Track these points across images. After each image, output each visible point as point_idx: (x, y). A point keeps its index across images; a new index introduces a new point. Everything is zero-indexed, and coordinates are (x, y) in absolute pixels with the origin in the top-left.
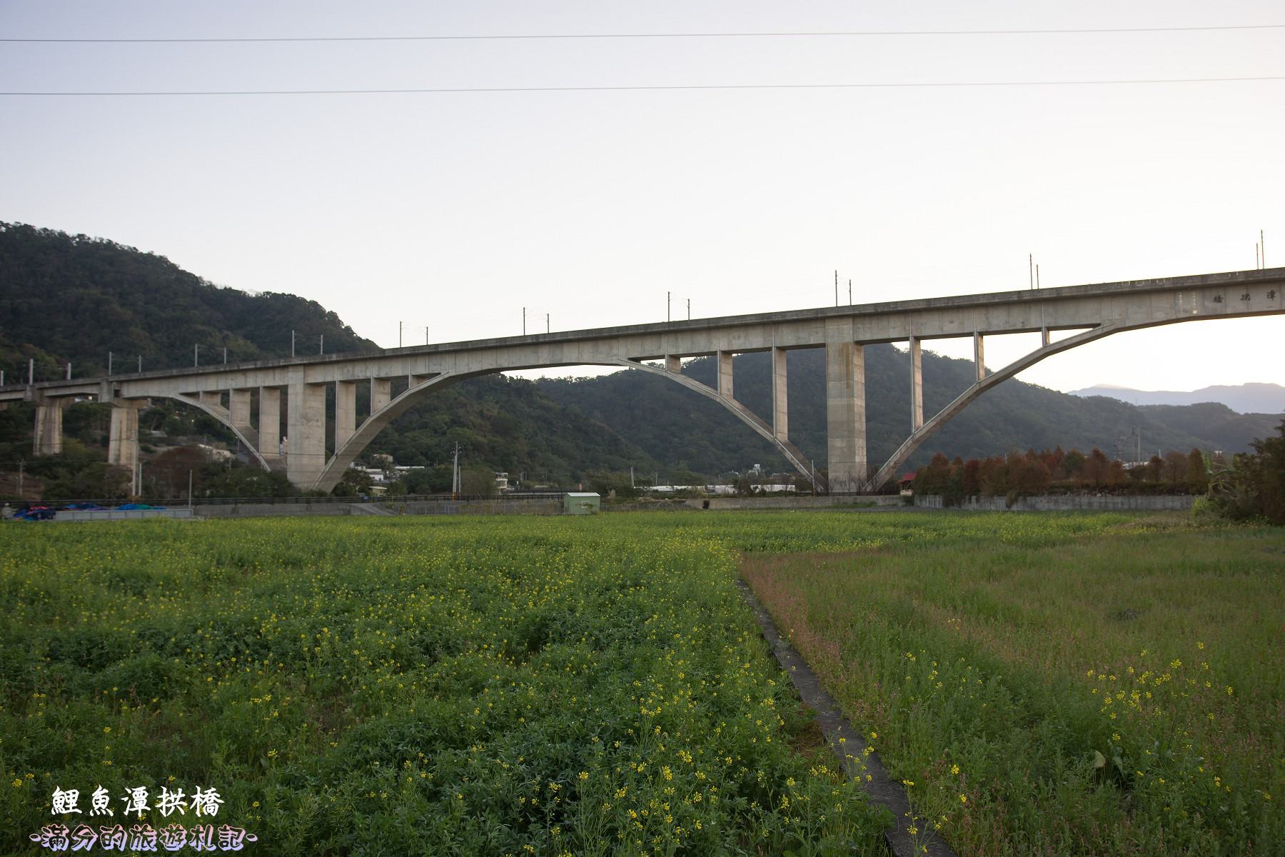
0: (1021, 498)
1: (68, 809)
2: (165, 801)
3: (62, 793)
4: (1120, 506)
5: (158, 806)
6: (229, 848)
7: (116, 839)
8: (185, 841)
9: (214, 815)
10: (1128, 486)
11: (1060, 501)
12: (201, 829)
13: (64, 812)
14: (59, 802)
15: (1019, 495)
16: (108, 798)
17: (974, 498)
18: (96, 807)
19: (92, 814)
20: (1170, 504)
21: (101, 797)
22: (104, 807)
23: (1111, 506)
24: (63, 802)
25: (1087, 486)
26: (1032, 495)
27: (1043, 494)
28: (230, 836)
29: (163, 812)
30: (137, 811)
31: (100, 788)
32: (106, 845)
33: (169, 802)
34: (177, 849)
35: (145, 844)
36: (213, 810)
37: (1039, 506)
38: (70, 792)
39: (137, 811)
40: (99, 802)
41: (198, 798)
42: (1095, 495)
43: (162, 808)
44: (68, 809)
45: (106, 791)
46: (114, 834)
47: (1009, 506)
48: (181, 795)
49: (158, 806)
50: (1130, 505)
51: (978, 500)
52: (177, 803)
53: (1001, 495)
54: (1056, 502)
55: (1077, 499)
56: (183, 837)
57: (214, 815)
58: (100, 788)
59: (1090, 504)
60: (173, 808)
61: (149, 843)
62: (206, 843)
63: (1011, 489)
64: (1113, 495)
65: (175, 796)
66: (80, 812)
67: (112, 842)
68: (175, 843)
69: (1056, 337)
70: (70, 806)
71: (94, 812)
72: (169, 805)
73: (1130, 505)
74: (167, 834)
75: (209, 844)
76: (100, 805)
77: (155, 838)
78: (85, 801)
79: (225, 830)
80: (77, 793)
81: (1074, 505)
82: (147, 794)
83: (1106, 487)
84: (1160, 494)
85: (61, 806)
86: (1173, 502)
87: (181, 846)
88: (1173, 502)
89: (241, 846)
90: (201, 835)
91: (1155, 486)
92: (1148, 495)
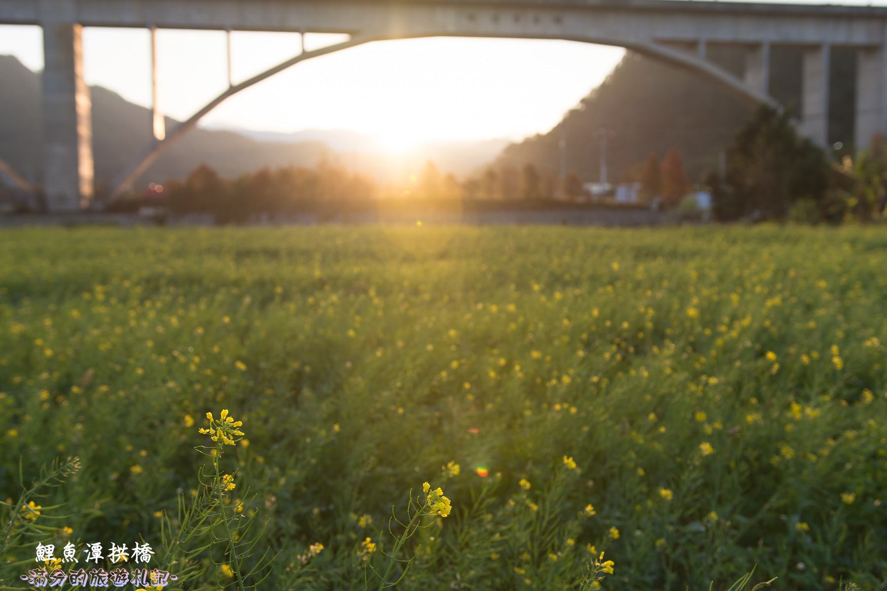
3: (43, 547)
9: (148, 562)
16: (74, 551)
18: (66, 556)
22: (72, 556)
29: (113, 560)
31: (69, 543)
33: (117, 553)
34: (122, 585)
35: (100, 582)
36: (146, 558)
38: (48, 546)
41: (136, 550)
48: (125, 548)
56: (127, 577)
57: (148, 562)
58: (69, 543)
61: (103, 581)
65: (121, 549)
69: (315, 41)
72: (116, 555)
76: (69, 555)
85: (42, 556)
87: (125, 583)
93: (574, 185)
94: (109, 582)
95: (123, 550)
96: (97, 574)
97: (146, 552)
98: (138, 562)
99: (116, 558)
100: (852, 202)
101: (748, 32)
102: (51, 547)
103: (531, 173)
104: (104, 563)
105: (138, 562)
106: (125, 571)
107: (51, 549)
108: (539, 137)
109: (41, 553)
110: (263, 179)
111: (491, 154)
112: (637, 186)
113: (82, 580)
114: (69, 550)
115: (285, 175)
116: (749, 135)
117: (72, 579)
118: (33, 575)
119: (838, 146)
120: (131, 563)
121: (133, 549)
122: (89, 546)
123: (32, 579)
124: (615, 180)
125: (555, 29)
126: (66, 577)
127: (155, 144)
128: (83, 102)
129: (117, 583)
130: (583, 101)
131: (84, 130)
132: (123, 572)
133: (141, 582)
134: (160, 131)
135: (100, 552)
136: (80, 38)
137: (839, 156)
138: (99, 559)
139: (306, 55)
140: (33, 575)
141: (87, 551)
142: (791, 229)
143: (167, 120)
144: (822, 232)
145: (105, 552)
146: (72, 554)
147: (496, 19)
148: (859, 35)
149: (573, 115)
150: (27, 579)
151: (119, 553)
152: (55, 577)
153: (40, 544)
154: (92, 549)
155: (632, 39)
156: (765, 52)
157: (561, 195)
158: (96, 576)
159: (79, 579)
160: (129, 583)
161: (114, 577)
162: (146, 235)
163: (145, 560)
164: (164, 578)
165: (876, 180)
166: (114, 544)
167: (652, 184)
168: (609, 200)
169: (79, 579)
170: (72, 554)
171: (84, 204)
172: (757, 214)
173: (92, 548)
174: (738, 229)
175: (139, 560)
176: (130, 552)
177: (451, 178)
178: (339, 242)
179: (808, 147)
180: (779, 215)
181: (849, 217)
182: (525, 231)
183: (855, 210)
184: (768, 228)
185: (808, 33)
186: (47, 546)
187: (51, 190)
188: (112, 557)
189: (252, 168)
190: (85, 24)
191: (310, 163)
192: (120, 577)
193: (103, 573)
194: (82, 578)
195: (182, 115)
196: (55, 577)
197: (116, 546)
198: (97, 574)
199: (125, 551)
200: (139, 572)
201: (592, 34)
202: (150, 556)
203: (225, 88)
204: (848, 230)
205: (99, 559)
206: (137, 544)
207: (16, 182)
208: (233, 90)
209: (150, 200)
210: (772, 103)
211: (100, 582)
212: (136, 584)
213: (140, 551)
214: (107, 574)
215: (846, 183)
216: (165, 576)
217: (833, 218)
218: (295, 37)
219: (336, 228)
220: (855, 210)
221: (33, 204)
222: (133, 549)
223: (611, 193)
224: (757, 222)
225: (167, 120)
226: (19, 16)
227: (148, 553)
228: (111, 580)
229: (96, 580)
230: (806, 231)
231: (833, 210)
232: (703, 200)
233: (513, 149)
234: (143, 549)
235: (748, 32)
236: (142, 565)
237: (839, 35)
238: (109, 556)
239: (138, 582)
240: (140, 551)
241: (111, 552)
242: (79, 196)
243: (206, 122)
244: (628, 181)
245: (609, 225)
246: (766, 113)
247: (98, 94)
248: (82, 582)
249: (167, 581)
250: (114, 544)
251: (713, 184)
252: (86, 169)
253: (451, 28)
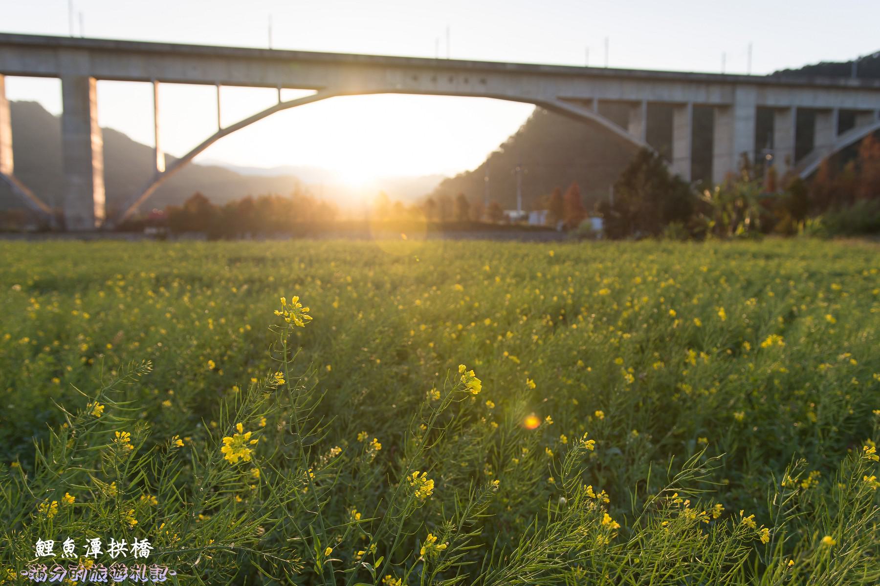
1: (47, 553)
3: (42, 542)
9: (146, 557)
13: (44, 555)
16: (74, 546)
18: (66, 552)
22: (71, 551)
28: (157, 572)
29: (112, 555)
31: (69, 539)
33: (116, 548)
34: (121, 580)
35: (100, 577)
36: (145, 554)
38: (48, 541)
41: (135, 545)
44: (47, 553)
45: (72, 541)
48: (124, 544)
52: (121, 549)
56: (125, 572)
57: (146, 557)
58: (69, 539)
60: (119, 553)
61: (102, 576)
62: (141, 577)
65: (120, 544)
68: (120, 577)
69: (289, 95)
70: (48, 551)
72: (115, 551)
76: (68, 551)
77: (106, 573)
85: (42, 551)
87: (124, 578)
93: (496, 211)
94: (108, 578)
95: (122, 545)
96: (97, 569)
97: (145, 548)
98: (136, 557)
99: (115, 553)
100: (712, 224)
101: (631, 93)
102: (51, 542)
103: (463, 201)
104: (102, 560)
105: (136, 557)
106: (124, 566)
107: (50, 544)
108: (468, 173)
109: (40, 548)
110: (247, 204)
111: (430, 187)
112: (546, 212)
113: (82, 575)
114: (69, 545)
115: (266, 202)
116: (633, 171)
117: (71, 574)
118: (33, 571)
119: (700, 182)
120: (128, 560)
121: (132, 545)
122: (89, 541)
123: (32, 574)
124: (528, 208)
125: (481, 89)
126: (66, 572)
127: (158, 176)
128: (97, 141)
129: (116, 578)
130: (503, 146)
131: (98, 164)
132: (122, 567)
133: (139, 577)
134: (161, 166)
135: (100, 548)
136: (95, 88)
137: (702, 191)
138: (98, 555)
139: (282, 106)
140: (33, 571)
141: (86, 546)
142: (666, 244)
143: (167, 156)
144: (690, 245)
145: (104, 547)
146: (71, 549)
147: (434, 80)
148: (715, 96)
149: (495, 155)
150: (26, 574)
151: (117, 547)
152: (55, 572)
153: (40, 539)
154: (92, 545)
155: (541, 98)
156: (644, 108)
157: (486, 219)
158: (95, 571)
159: (79, 574)
160: (128, 579)
161: (113, 572)
162: (152, 248)
163: (144, 555)
164: (162, 573)
165: (730, 207)
166: (113, 540)
167: (557, 211)
168: (523, 223)
169: (79, 574)
170: (71, 549)
171: (98, 224)
172: (638, 234)
173: (91, 543)
174: (625, 244)
175: (138, 555)
176: (129, 546)
177: (398, 205)
178: (312, 252)
179: (677, 181)
180: (656, 233)
181: (709, 235)
182: (460, 244)
183: (713, 230)
184: (648, 243)
185: (677, 94)
186: (47, 542)
187: (69, 213)
188: (111, 552)
189: (237, 196)
190: (98, 78)
191: (286, 193)
192: (119, 572)
193: (102, 568)
194: (81, 573)
195: (179, 153)
196: (55, 572)
197: (115, 542)
198: (97, 569)
199: (124, 546)
200: (138, 567)
201: (510, 93)
202: (149, 551)
203: (214, 130)
204: (710, 244)
205: (98, 555)
206: (136, 539)
207: (41, 206)
208: (222, 133)
209: (152, 221)
210: (651, 149)
211: (100, 577)
212: (135, 579)
213: (139, 546)
214: (106, 569)
215: (707, 209)
216: (164, 570)
217: (699, 236)
218: (273, 91)
219: (310, 242)
220: (713, 230)
221: (53, 224)
222: (132, 545)
223: (526, 218)
224: (639, 239)
225: (167, 156)
226: (42, 69)
227: (147, 548)
228: (111, 575)
229: (95, 575)
230: (677, 245)
231: (696, 230)
232: (597, 223)
233: (447, 182)
234: (141, 545)
235: (631, 93)
236: (141, 560)
237: (700, 96)
238: (109, 551)
239: (137, 577)
240: (139, 546)
241: (110, 547)
242: (93, 218)
243: (198, 159)
244: (539, 208)
245: (525, 240)
246: (645, 155)
247: (108, 134)
248: (81, 577)
249: (166, 576)
250: (113, 540)
251: (605, 211)
252: (99, 195)
253: (399, 87)
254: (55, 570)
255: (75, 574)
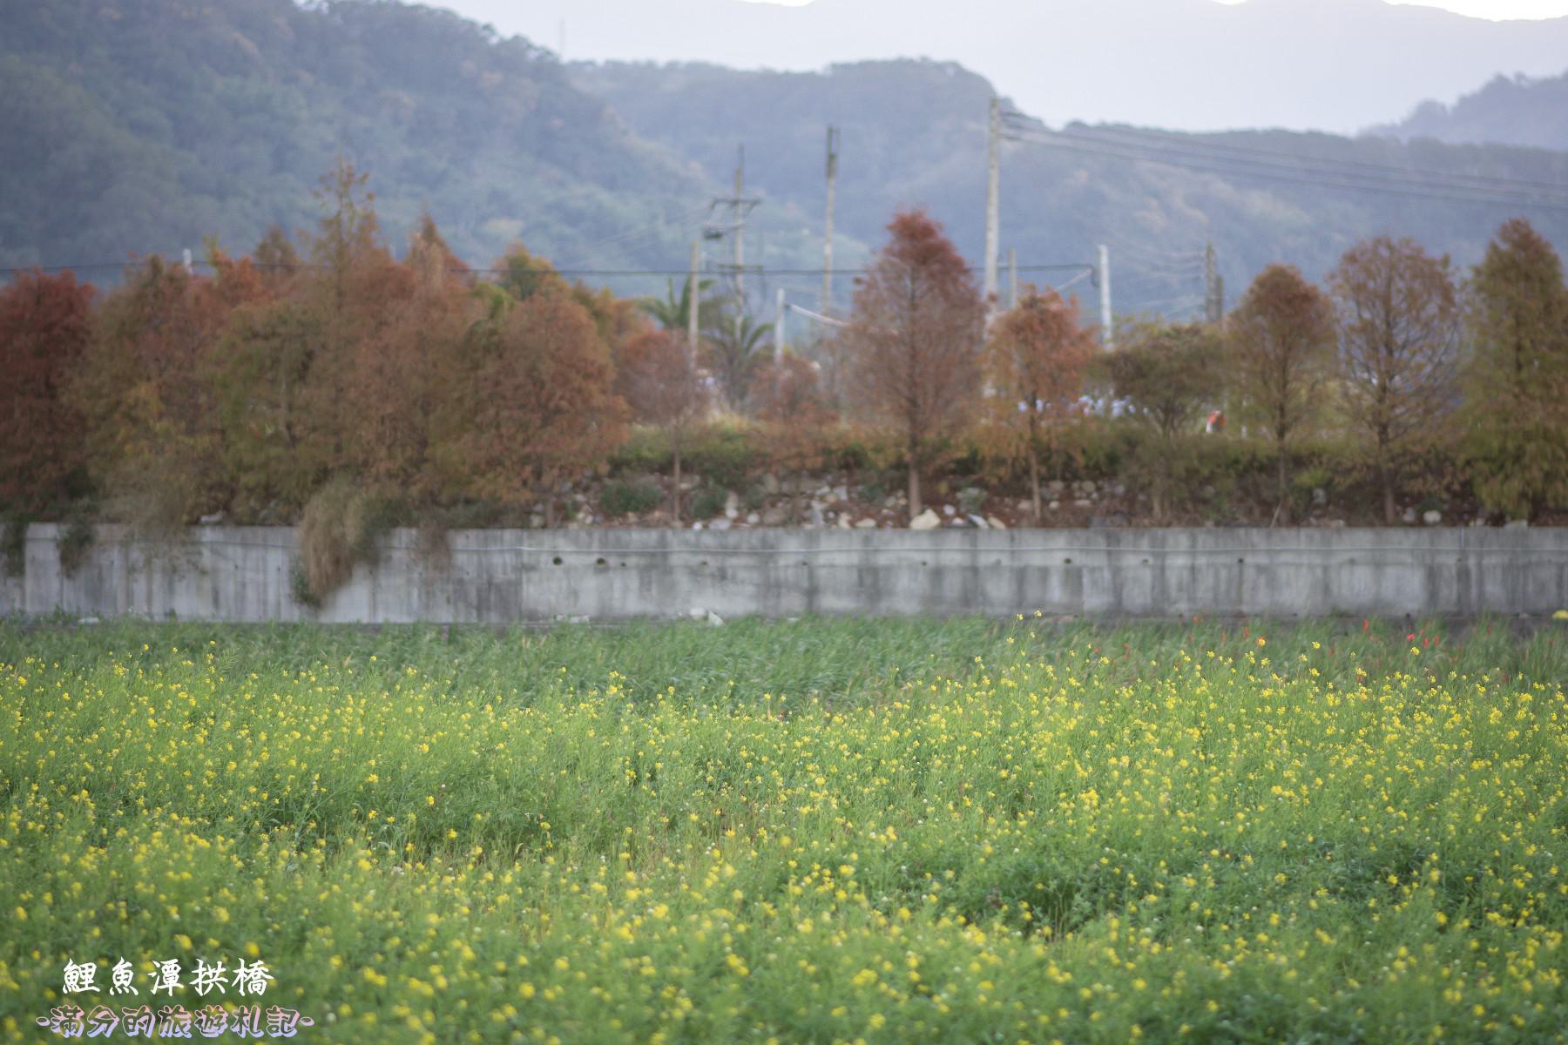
0: (404, 537)
2: (201, 976)
3: (75, 967)
4: (1057, 593)
5: (193, 983)
6: (280, 1033)
7: (143, 1025)
8: (226, 1026)
9: (261, 993)
10: (1105, 467)
11: (679, 559)
12: (246, 1011)
13: (78, 990)
14: (72, 977)
15: (390, 516)
16: (131, 974)
17: (44, 540)
18: (117, 984)
19: (112, 993)
20: (1356, 585)
21: (123, 972)
22: (127, 984)
23: (999, 590)
24: (77, 978)
25: (849, 463)
26: (491, 517)
27: (564, 514)
28: (280, 1020)
29: (199, 991)
30: (167, 989)
31: (122, 960)
32: (129, 1031)
33: (207, 978)
34: (216, 1035)
35: (177, 1029)
36: (259, 988)
37: (540, 593)
38: (86, 966)
39: (167, 989)
40: (122, 978)
41: (241, 972)
42: (902, 520)
43: (197, 985)
45: (129, 964)
46: (139, 1017)
47: (310, 595)
48: (220, 970)
49: (193, 983)
50: (1117, 590)
51: (74, 552)
52: (216, 979)
53: (253, 520)
54: (656, 565)
55: (791, 546)
56: (224, 1020)
57: (261, 993)
59: (871, 581)
60: (211, 986)
62: (252, 1027)
63: (323, 475)
64: (1013, 521)
65: (213, 970)
66: (98, 990)
67: (137, 1026)
70: (86, 983)
71: (115, 990)
72: (206, 982)
73: (1117, 590)
74: (204, 1017)
75: (255, 1030)
76: (122, 982)
77: (189, 1022)
78: (104, 978)
79: (274, 1011)
80: (94, 967)
81: (771, 588)
82: (179, 968)
83: (967, 468)
84: (1295, 520)
86: (1378, 565)
87: (221, 1031)
88: (1378, 565)
89: (295, 1031)
90: (245, 1019)
91: (1267, 467)
92: (1226, 522)
202: (265, 983)
254: (99, 1016)
255: (134, 1024)
